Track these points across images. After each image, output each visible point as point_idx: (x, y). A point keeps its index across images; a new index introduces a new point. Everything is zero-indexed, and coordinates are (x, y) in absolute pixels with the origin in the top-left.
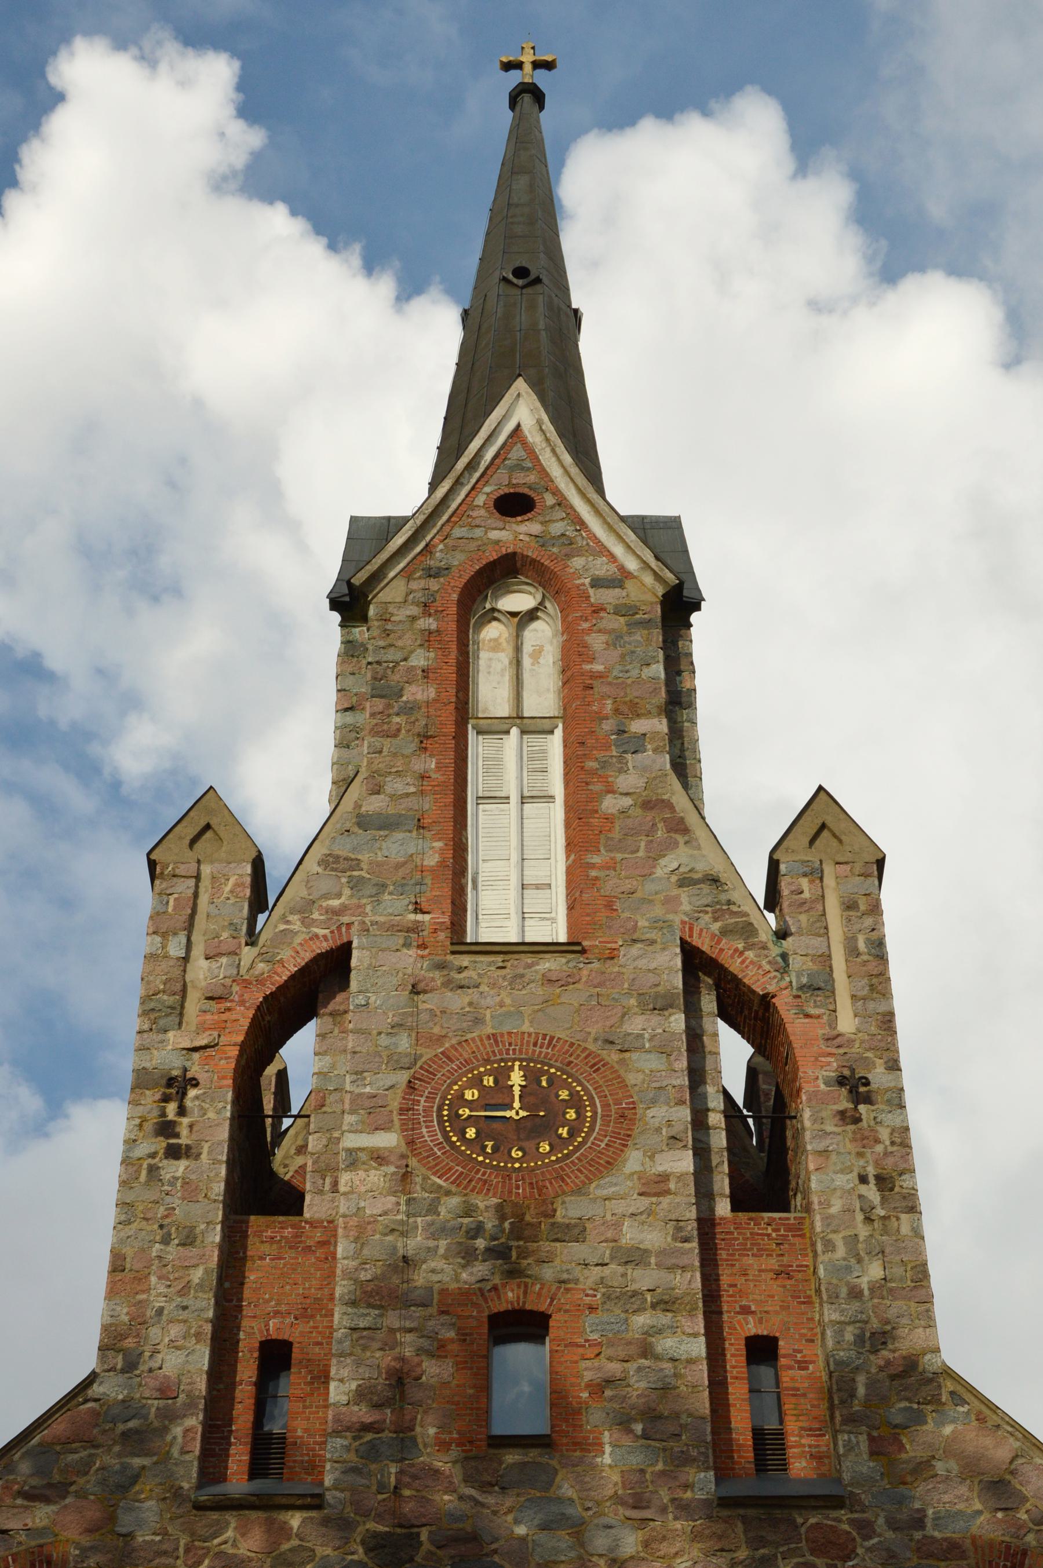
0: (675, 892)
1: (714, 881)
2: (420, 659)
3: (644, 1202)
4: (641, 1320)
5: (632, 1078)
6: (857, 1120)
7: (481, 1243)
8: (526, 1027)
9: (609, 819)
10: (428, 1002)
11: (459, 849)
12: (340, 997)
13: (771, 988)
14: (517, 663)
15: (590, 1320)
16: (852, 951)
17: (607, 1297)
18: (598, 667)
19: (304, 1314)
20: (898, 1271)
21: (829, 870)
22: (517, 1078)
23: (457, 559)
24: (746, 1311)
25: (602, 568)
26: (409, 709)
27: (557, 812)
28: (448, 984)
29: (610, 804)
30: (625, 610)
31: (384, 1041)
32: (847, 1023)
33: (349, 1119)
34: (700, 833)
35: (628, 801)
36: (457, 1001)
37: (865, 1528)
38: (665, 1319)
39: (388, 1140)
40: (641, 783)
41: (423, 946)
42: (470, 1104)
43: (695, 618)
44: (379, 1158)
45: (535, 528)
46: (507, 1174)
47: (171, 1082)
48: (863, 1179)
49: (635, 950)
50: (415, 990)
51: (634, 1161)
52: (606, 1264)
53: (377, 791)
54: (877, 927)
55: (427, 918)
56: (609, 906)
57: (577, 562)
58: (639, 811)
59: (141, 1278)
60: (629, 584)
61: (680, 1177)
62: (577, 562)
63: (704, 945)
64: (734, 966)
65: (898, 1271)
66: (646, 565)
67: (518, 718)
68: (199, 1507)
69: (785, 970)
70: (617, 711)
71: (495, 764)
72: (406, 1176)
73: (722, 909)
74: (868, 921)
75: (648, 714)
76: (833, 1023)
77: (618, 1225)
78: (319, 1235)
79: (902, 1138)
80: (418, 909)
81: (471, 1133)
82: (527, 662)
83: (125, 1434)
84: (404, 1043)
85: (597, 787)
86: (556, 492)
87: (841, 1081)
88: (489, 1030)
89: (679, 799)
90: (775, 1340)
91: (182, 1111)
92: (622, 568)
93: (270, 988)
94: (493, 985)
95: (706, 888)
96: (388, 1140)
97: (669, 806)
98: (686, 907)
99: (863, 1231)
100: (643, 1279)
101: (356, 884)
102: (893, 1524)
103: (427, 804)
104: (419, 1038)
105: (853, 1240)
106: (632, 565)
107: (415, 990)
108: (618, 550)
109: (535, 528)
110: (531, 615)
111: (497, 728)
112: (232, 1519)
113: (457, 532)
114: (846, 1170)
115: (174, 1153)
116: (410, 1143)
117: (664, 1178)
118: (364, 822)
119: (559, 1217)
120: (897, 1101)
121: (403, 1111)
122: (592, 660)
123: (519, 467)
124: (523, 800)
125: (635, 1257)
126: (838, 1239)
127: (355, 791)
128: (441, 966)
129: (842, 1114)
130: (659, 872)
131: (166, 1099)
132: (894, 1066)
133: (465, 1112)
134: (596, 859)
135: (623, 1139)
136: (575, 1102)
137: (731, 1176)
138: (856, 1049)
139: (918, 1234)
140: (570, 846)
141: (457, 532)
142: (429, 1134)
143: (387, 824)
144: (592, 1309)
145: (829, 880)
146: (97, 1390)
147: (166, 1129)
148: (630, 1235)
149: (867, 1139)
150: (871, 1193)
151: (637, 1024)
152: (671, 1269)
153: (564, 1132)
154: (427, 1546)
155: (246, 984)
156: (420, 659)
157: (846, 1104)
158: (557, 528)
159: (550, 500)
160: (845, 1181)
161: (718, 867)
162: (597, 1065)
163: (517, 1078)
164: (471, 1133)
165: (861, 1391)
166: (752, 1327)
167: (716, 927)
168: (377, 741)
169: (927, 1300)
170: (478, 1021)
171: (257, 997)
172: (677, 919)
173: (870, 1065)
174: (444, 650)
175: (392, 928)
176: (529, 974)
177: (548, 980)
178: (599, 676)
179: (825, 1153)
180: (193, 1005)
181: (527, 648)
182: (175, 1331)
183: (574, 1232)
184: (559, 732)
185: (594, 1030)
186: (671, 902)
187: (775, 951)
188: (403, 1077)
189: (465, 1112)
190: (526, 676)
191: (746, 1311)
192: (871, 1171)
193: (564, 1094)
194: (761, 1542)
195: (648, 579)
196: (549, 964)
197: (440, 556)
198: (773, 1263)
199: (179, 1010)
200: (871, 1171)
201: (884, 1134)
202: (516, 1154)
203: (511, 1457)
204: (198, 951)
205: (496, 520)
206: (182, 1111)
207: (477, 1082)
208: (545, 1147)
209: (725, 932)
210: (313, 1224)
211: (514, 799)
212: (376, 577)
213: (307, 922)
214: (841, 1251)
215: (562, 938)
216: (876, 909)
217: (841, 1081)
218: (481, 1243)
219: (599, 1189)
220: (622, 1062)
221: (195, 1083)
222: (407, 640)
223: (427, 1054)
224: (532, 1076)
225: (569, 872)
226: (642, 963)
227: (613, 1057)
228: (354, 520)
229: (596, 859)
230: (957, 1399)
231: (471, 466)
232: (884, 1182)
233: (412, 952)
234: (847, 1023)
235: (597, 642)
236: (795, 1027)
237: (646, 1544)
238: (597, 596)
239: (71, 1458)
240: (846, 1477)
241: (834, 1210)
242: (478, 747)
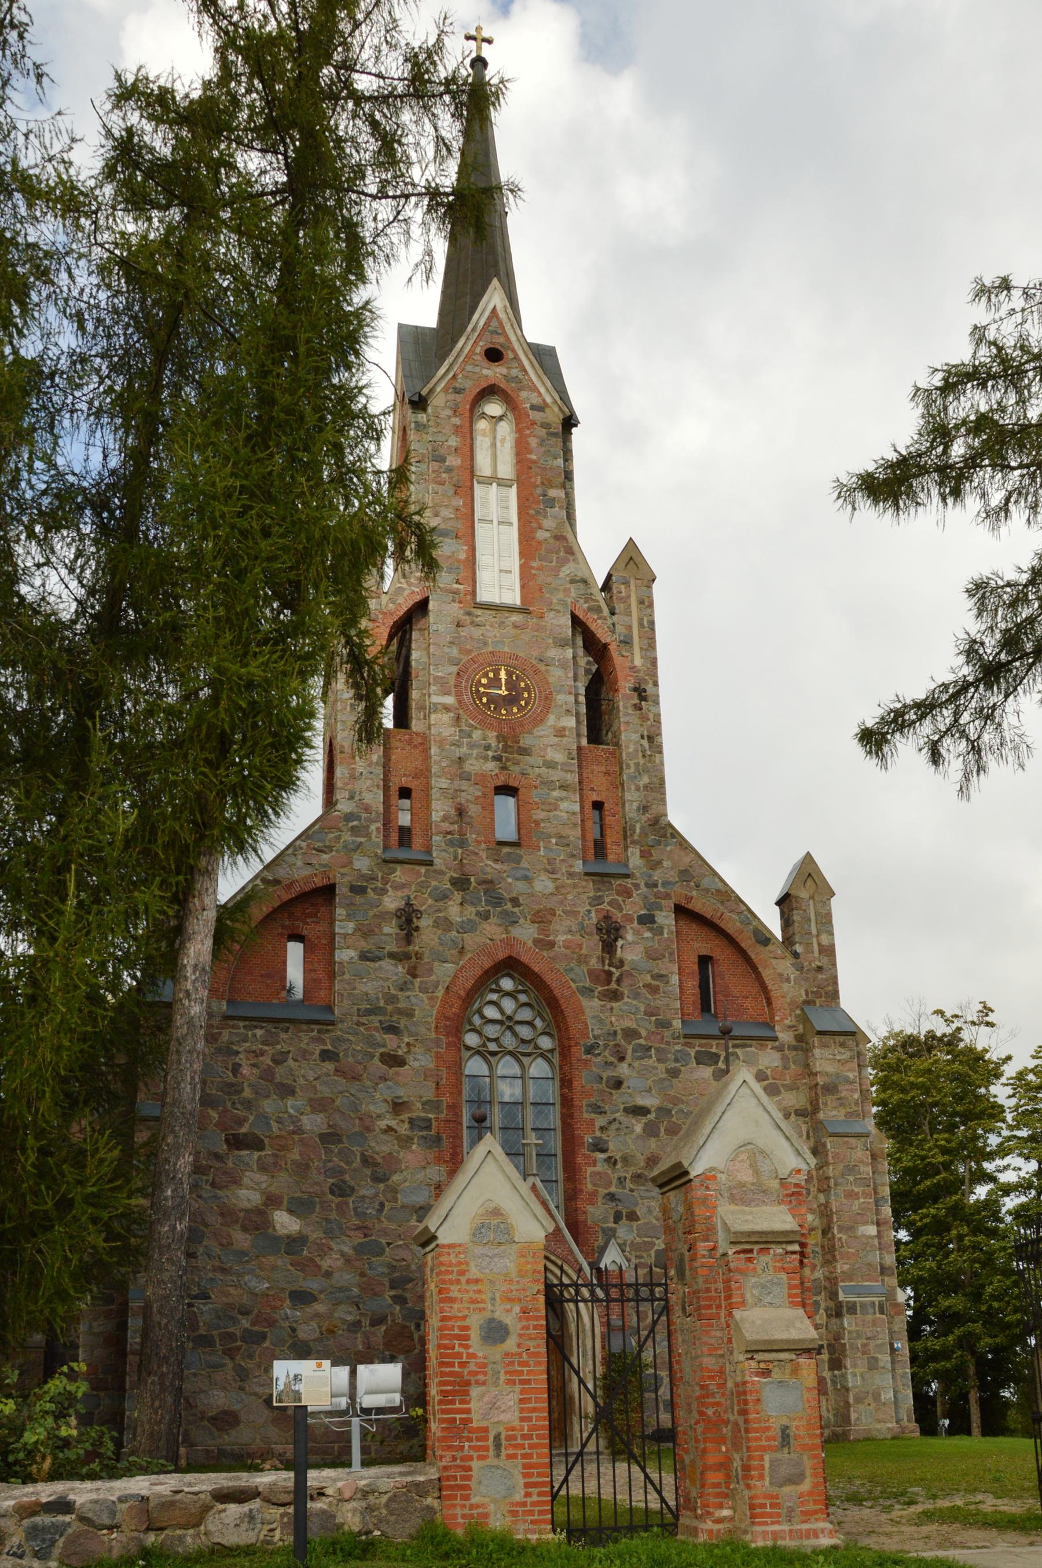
0: (568, 586)
4: (556, 794)
5: (551, 680)
6: (641, 709)
7: (490, 753)
8: (506, 649)
9: (540, 543)
10: (464, 632)
12: (423, 621)
13: (608, 640)
15: (534, 792)
16: (641, 625)
17: (542, 783)
18: (534, 457)
19: (416, 777)
21: (632, 582)
22: (503, 675)
23: (468, 384)
24: (592, 789)
25: (536, 400)
26: (449, 470)
28: (472, 623)
29: (541, 535)
30: (546, 426)
31: (446, 650)
32: (638, 661)
33: (433, 688)
34: (579, 555)
35: (547, 535)
36: (477, 633)
37: (637, 886)
38: (564, 794)
39: (450, 700)
40: (554, 525)
41: (460, 602)
42: (484, 686)
43: (574, 430)
44: (447, 709)
46: (500, 721)
48: (642, 737)
49: (552, 614)
50: (458, 625)
51: (551, 719)
52: (421, 607)
53: (436, 515)
54: (651, 615)
55: (461, 587)
56: (540, 590)
57: (524, 394)
58: (552, 541)
60: (547, 410)
61: (571, 729)
63: (581, 615)
64: (593, 627)
66: (555, 402)
68: (385, 861)
69: (613, 632)
70: (543, 483)
71: (486, 503)
72: (458, 718)
73: (588, 598)
74: (649, 611)
75: (556, 487)
76: (632, 661)
77: (545, 750)
78: (420, 740)
79: (658, 720)
80: (457, 582)
81: (484, 700)
82: (498, 444)
84: (455, 652)
85: (534, 525)
86: (513, 351)
87: (635, 689)
88: (490, 649)
92: (544, 401)
93: (396, 618)
94: (492, 626)
95: (582, 586)
96: (450, 700)
98: (573, 595)
99: (642, 761)
100: (556, 775)
102: (647, 885)
103: (459, 525)
105: (637, 765)
106: (549, 400)
107: (458, 625)
108: (542, 390)
110: (501, 418)
112: (399, 867)
113: (469, 368)
114: (636, 732)
116: (460, 702)
117: (564, 729)
119: (521, 744)
120: (657, 703)
121: (456, 686)
122: (531, 452)
124: (500, 523)
125: (551, 765)
126: (631, 763)
128: (469, 614)
129: (635, 705)
130: (562, 575)
132: (656, 684)
133: (482, 690)
134: (534, 564)
135: (547, 709)
137: (588, 726)
138: (642, 674)
139: (662, 764)
140: (522, 554)
141: (469, 368)
142: (467, 699)
145: (633, 587)
149: (644, 718)
150: (645, 743)
151: (553, 653)
152: (567, 771)
153: (523, 703)
154: (474, 884)
155: (384, 614)
157: (636, 701)
158: (514, 372)
159: (511, 355)
160: (635, 737)
161: (586, 575)
162: (537, 672)
163: (503, 675)
164: (484, 700)
165: (638, 831)
166: (595, 797)
167: (586, 606)
168: (436, 487)
169: (664, 794)
170: (485, 644)
171: (390, 622)
172: (569, 600)
173: (646, 682)
176: (507, 622)
178: (534, 462)
179: (627, 723)
181: (499, 437)
182: (369, 783)
184: (515, 487)
185: (535, 654)
186: (567, 591)
187: (610, 622)
190: (498, 453)
191: (592, 789)
192: (646, 733)
193: (522, 685)
194: (599, 890)
195: (556, 409)
197: (460, 382)
200: (646, 733)
201: (651, 716)
202: (503, 712)
203: (506, 850)
205: (485, 363)
207: (486, 675)
208: (515, 710)
209: (590, 609)
210: (418, 734)
211: (495, 522)
212: (431, 391)
214: (632, 770)
215: (518, 602)
217: (635, 689)
218: (490, 753)
219: (539, 731)
220: (547, 671)
222: (447, 430)
223: (465, 658)
224: (509, 674)
225: (521, 567)
226: (554, 621)
227: (542, 667)
228: (401, 327)
229: (534, 564)
230: (673, 836)
231: (474, 329)
232: (650, 739)
233: (456, 605)
234: (638, 661)
235: (533, 442)
236: (618, 660)
237: (557, 888)
238: (534, 415)
239: (332, 835)
240: (631, 866)
241: (631, 750)
242: (479, 490)
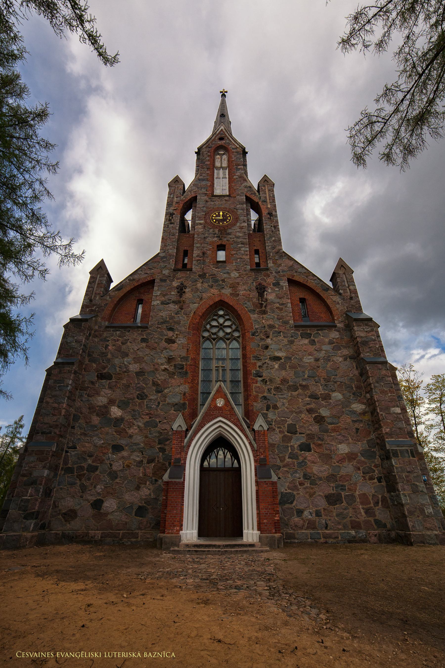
1: (250, 187)
2: (208, 158)
3: (240, 230)
5: (238, 213)
6: (271, 219)
9: (235, 179)
10: (209, 203)
11: (213, 184)
14: (221, 160)
16: (270, 196)
20: (277, 239)
21: (266, 186)
22: (221, 213)
26: (206, 165)
27: (227, 179)
28: (211, 201)
30: (237, 152)
36: (212, 203)
37: (272, 273)
38: (243, 245)
39: (202, 222)
42: (214, 217)
44: (201, 224)
45: (224, 142)
47: (171, 214)
51: (238, 224)
53: (201, 176)
59: (166, 240)
62: (230, 146)
65: (277, 239)
67: (221, 167)
79: (277, 222)
81: (214, 221)
82: (223, 160)
83: (322, 441)
84: (205, 209)
89: (245, 177)
90: (258, 250)
91: (172, 218)
96: (202, 222)
97: (243, 177)
100: (239, 240)
101: (198, 188)
102: (276, 272)
104: (207, 208)
109: (224, 142)
111: (218, 169)
115: (171, 223)
116: (206, 222)
118: (199, 180)
123: (222, 134)
125: (238, 237)
127: (198, 175)
131: (170, 216)
132: (276, 212)
133: (213, 218)
136: (230, 216)
143: (203, 180)
144: (232, 244)
146: (160, 255)
147: (170, 220)
148: (238, 234)
152: (244, 239)
156: (208, 158)
158: (227, 142)
163: (221, 213)
164: (214, 221)
166: (255, 248)
171: (183, 203)
174: (211, 158)
175: (203, 194)
177: (226, 200)
178: (233, 161)
179: (266, 223)
180: (174, 203)
183: (229, 234)
188: (204, 213)
189: (213, 218)
196: (226, 198)
198: (258, 239)
199: (172, 204)
201: (275, 221)
202: (221, 223)
204: (175, 197)
206: (172, 218)
208: (225, 223)
209: (251, 194)
210: (191, 234)
213: (191, 193)
215: (228, 194)
216: (273, 191)
217: (268, 214)
218: (216, 235)
221: (174, 214)
237: (240, 275)
